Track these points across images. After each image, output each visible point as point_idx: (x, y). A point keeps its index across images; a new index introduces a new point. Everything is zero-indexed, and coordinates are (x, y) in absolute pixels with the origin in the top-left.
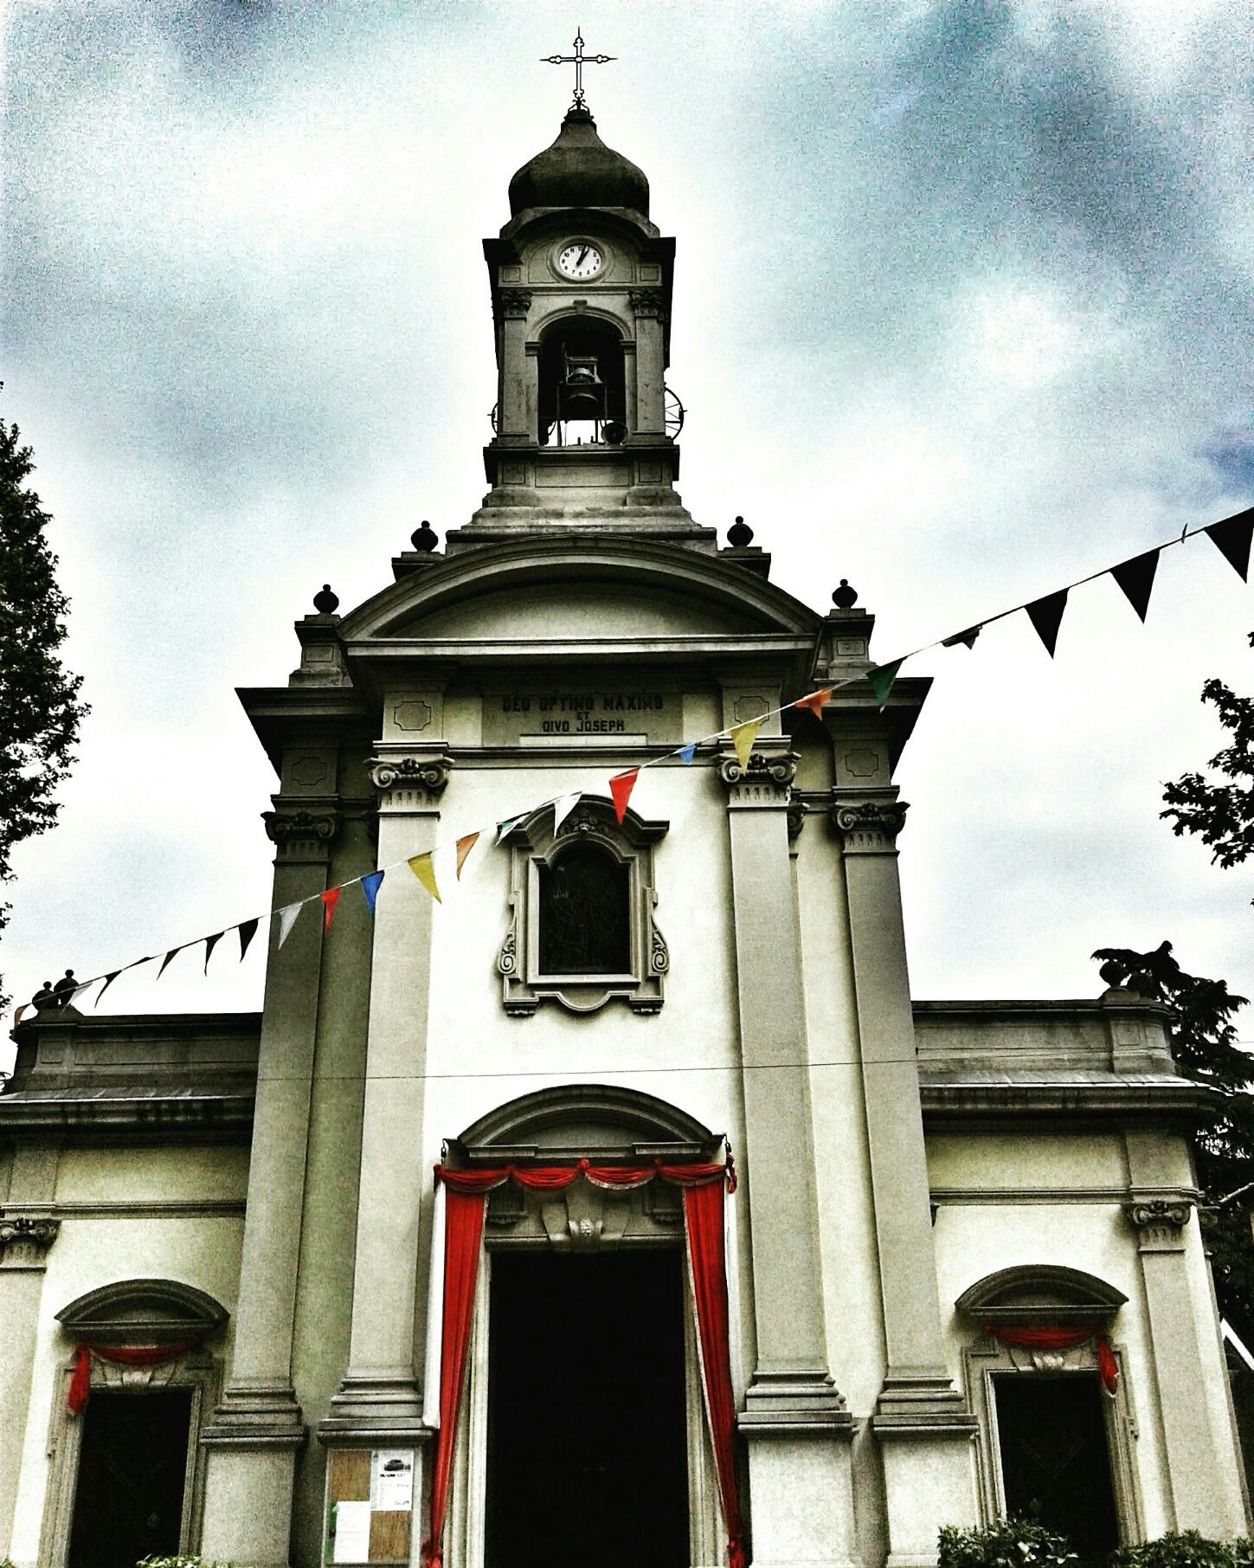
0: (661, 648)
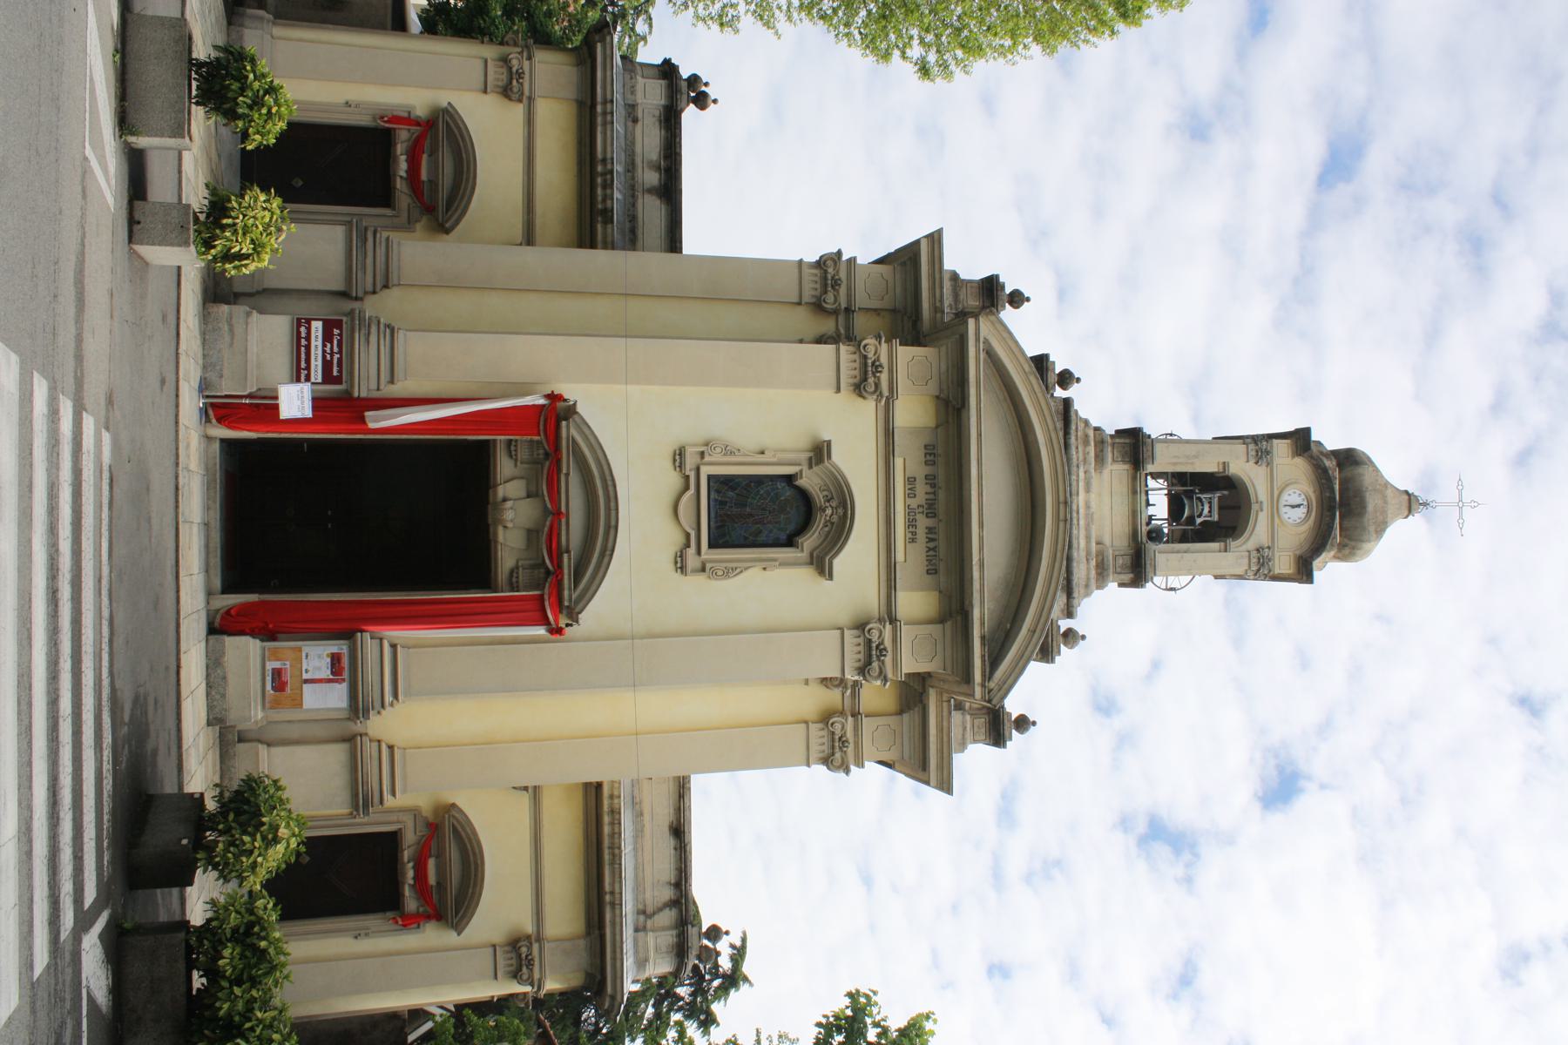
0: (976, 574)
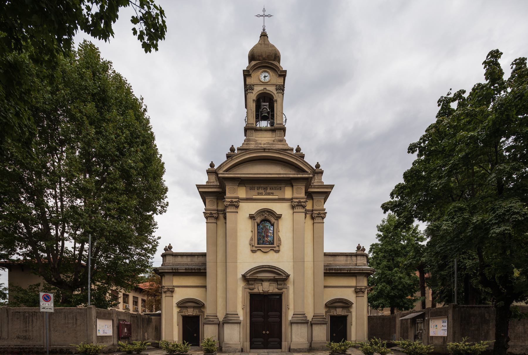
0: (282, 176)
